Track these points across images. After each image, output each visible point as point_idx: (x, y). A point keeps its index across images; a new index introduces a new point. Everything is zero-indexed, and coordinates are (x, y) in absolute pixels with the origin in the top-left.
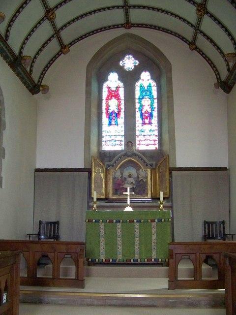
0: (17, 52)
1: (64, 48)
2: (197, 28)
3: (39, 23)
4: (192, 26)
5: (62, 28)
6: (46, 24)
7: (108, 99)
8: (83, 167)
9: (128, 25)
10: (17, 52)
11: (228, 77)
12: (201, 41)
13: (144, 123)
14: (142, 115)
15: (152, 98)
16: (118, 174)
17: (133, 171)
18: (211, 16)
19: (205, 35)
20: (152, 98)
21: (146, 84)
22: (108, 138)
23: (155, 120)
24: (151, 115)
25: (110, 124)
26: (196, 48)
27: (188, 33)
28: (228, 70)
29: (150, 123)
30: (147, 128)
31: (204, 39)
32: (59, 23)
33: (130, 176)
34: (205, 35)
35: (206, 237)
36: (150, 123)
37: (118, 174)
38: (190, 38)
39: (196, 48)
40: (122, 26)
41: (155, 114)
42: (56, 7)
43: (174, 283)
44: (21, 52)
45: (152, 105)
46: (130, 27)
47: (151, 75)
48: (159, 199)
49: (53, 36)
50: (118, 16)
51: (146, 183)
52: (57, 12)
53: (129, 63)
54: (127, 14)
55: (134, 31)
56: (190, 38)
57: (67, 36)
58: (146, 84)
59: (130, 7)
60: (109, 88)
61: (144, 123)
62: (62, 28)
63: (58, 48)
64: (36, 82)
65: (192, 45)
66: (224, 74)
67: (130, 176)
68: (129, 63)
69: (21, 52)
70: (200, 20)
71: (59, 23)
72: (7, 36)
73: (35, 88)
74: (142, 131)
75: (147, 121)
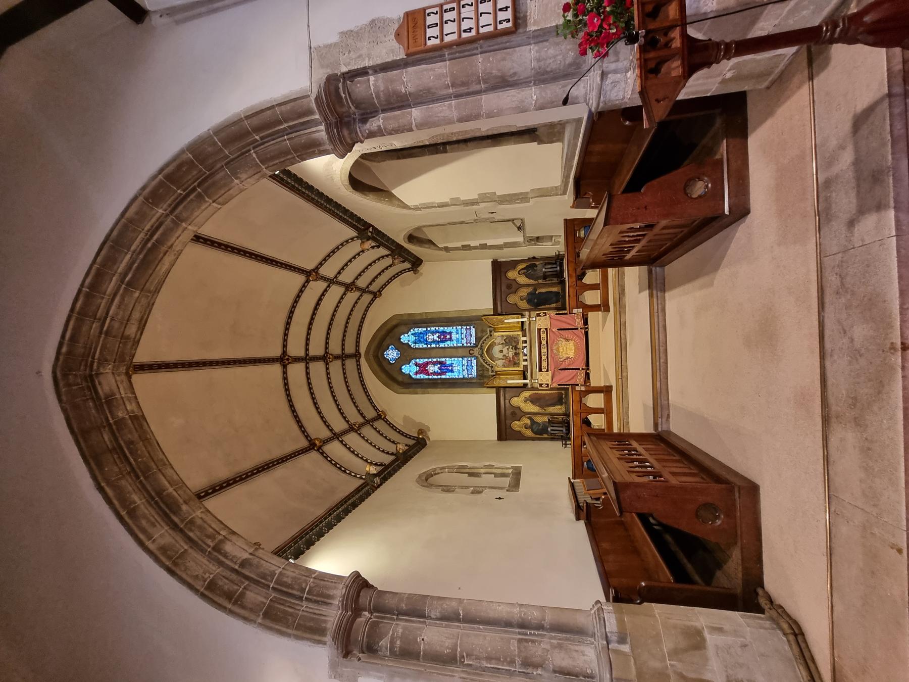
0: (393, 458)
1: (380, 416)
2: (331, 282)
3: (345, 445)
4: (361, 295)
5: (331, 430)
6: (327, 448)
7: (428, 374)
8: (495, 395)
9: (356, 355)
10: (393, 458)
11: (409, 261)
12: (374, 287)
13: (450, 339)
14: (442, 341)
15: (426, 332)
16: (500, 363)
17: (496, 349)
18: (321, 264)
19: (370, 284)
20: (426, 332)
21: (413, 338)
22: (465, 373)
23: (447, 329)
24: (443, 333)
25: (452, 371)
26: (380, 291)
27: (367, 298)
28: (378, 247)
29: (450, 333)
30: (454, 336)
31: (374, 284)
32: (325, 433)
33: (501, 351)
34: (370, 284)
35: (565, 438)
36: (450, 333)
37: (500, 363)
38: (371, 296)
39: (380, 291)
40: (358, 361)
41: (441, 329)
42: (348, 422)
43: (604, 307)
44: (392, 454)
45: (433, 333)
46: (360, 354)
47: (403, 334)
48: (523, 322)
49: (341, 442)
50: (296, 371)
51: (508, 337)
52: (352, 421)
53: (392, 354)
54: (315, 359)
55: (363, 350)
56: (371, 296)
57: (370, 414)
58: (413, 338)
59: (307, 355)
60: (416, 373)
61: (450, 339)
62: (331, 430)
63: (381, 421)
64: (414, 442)
65: (376, 295)
66: (407, 265)
67: (501, 351)
68: (392, 354)
69: (392, 454)
70: (324, 279)
71: (326, 434)
72: (381, 465)
73: (419, 443)
74: (457, 340)
75: (448, 337)
